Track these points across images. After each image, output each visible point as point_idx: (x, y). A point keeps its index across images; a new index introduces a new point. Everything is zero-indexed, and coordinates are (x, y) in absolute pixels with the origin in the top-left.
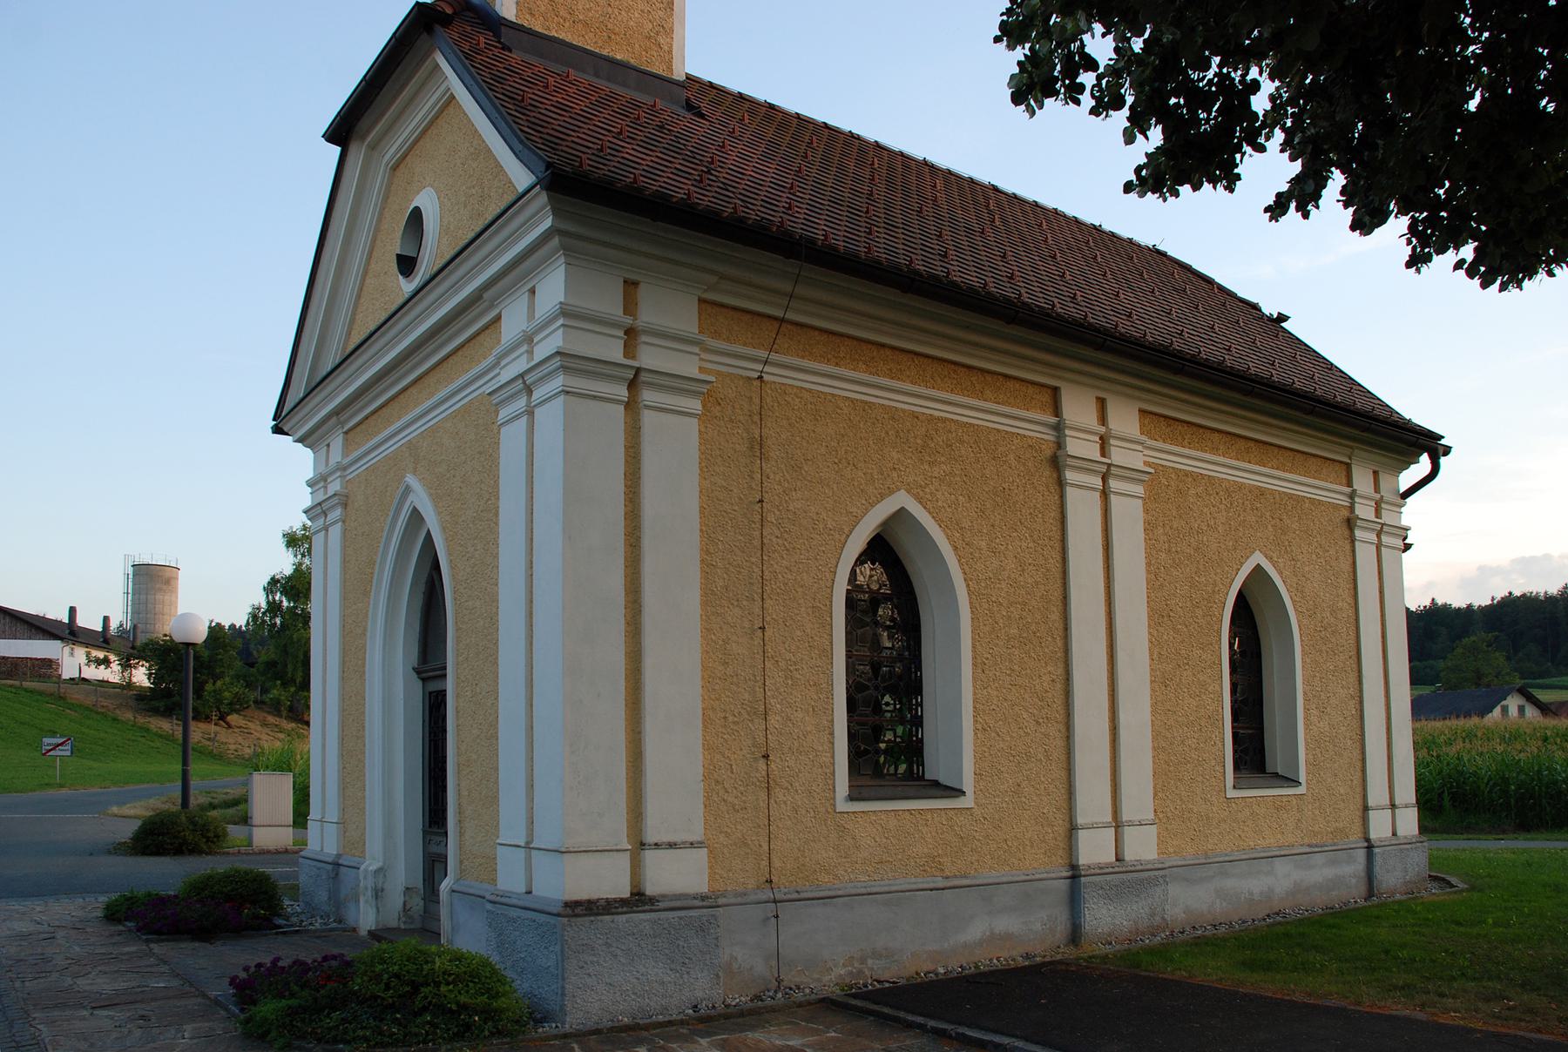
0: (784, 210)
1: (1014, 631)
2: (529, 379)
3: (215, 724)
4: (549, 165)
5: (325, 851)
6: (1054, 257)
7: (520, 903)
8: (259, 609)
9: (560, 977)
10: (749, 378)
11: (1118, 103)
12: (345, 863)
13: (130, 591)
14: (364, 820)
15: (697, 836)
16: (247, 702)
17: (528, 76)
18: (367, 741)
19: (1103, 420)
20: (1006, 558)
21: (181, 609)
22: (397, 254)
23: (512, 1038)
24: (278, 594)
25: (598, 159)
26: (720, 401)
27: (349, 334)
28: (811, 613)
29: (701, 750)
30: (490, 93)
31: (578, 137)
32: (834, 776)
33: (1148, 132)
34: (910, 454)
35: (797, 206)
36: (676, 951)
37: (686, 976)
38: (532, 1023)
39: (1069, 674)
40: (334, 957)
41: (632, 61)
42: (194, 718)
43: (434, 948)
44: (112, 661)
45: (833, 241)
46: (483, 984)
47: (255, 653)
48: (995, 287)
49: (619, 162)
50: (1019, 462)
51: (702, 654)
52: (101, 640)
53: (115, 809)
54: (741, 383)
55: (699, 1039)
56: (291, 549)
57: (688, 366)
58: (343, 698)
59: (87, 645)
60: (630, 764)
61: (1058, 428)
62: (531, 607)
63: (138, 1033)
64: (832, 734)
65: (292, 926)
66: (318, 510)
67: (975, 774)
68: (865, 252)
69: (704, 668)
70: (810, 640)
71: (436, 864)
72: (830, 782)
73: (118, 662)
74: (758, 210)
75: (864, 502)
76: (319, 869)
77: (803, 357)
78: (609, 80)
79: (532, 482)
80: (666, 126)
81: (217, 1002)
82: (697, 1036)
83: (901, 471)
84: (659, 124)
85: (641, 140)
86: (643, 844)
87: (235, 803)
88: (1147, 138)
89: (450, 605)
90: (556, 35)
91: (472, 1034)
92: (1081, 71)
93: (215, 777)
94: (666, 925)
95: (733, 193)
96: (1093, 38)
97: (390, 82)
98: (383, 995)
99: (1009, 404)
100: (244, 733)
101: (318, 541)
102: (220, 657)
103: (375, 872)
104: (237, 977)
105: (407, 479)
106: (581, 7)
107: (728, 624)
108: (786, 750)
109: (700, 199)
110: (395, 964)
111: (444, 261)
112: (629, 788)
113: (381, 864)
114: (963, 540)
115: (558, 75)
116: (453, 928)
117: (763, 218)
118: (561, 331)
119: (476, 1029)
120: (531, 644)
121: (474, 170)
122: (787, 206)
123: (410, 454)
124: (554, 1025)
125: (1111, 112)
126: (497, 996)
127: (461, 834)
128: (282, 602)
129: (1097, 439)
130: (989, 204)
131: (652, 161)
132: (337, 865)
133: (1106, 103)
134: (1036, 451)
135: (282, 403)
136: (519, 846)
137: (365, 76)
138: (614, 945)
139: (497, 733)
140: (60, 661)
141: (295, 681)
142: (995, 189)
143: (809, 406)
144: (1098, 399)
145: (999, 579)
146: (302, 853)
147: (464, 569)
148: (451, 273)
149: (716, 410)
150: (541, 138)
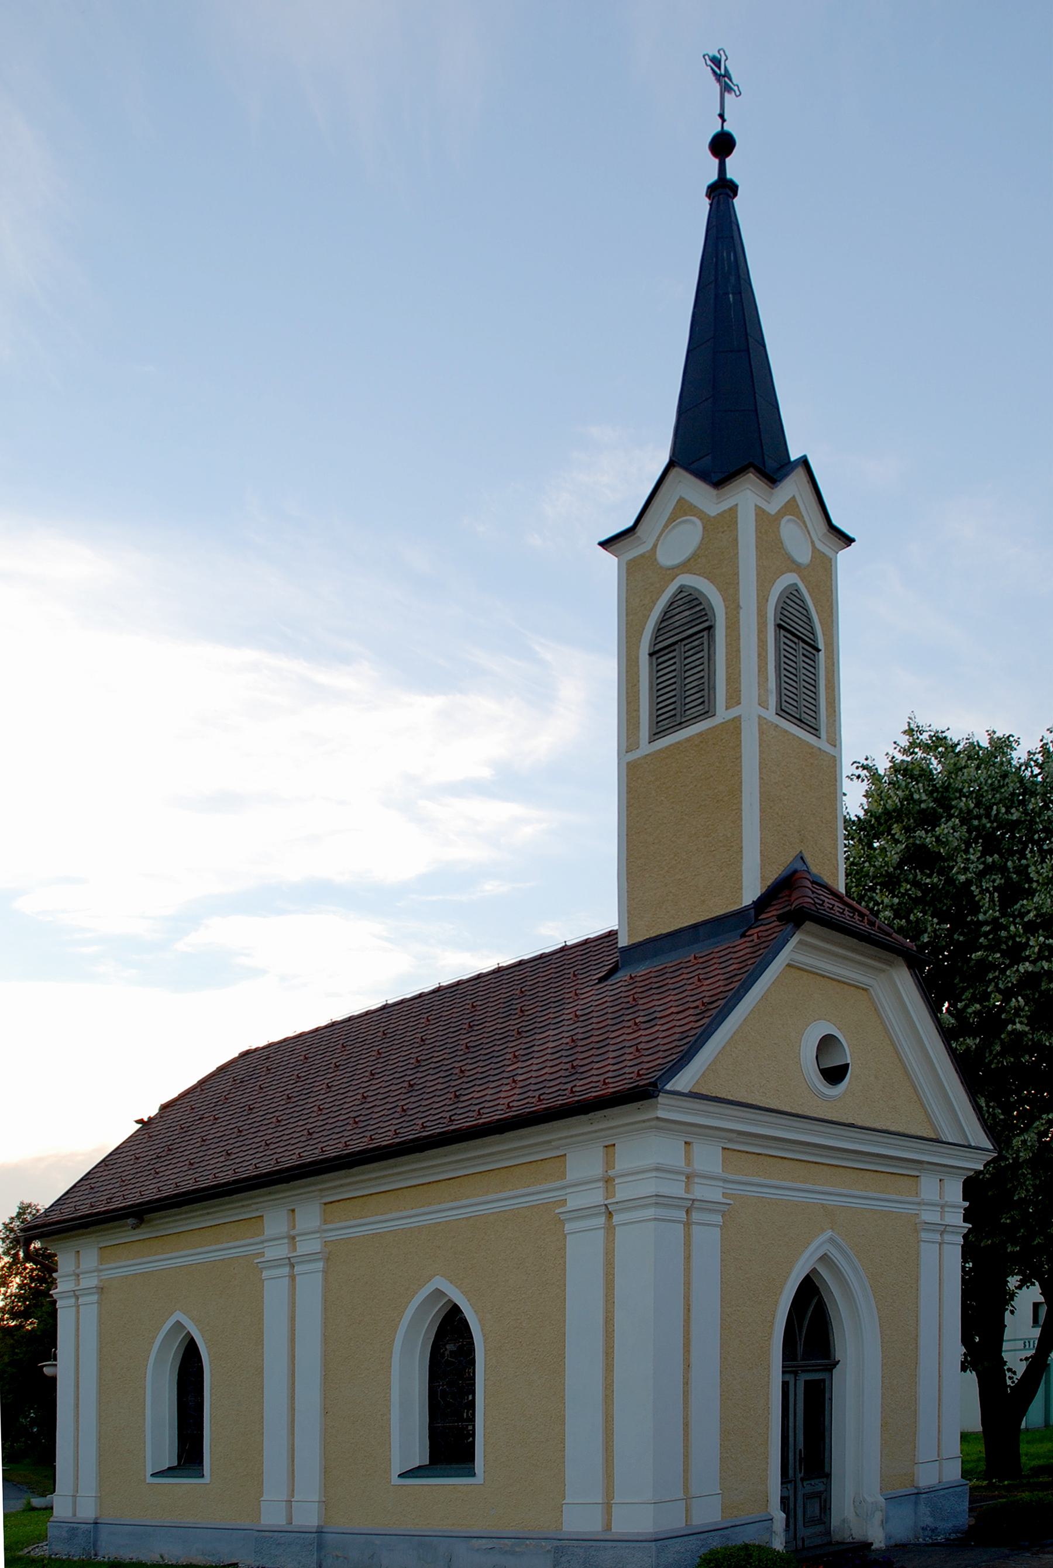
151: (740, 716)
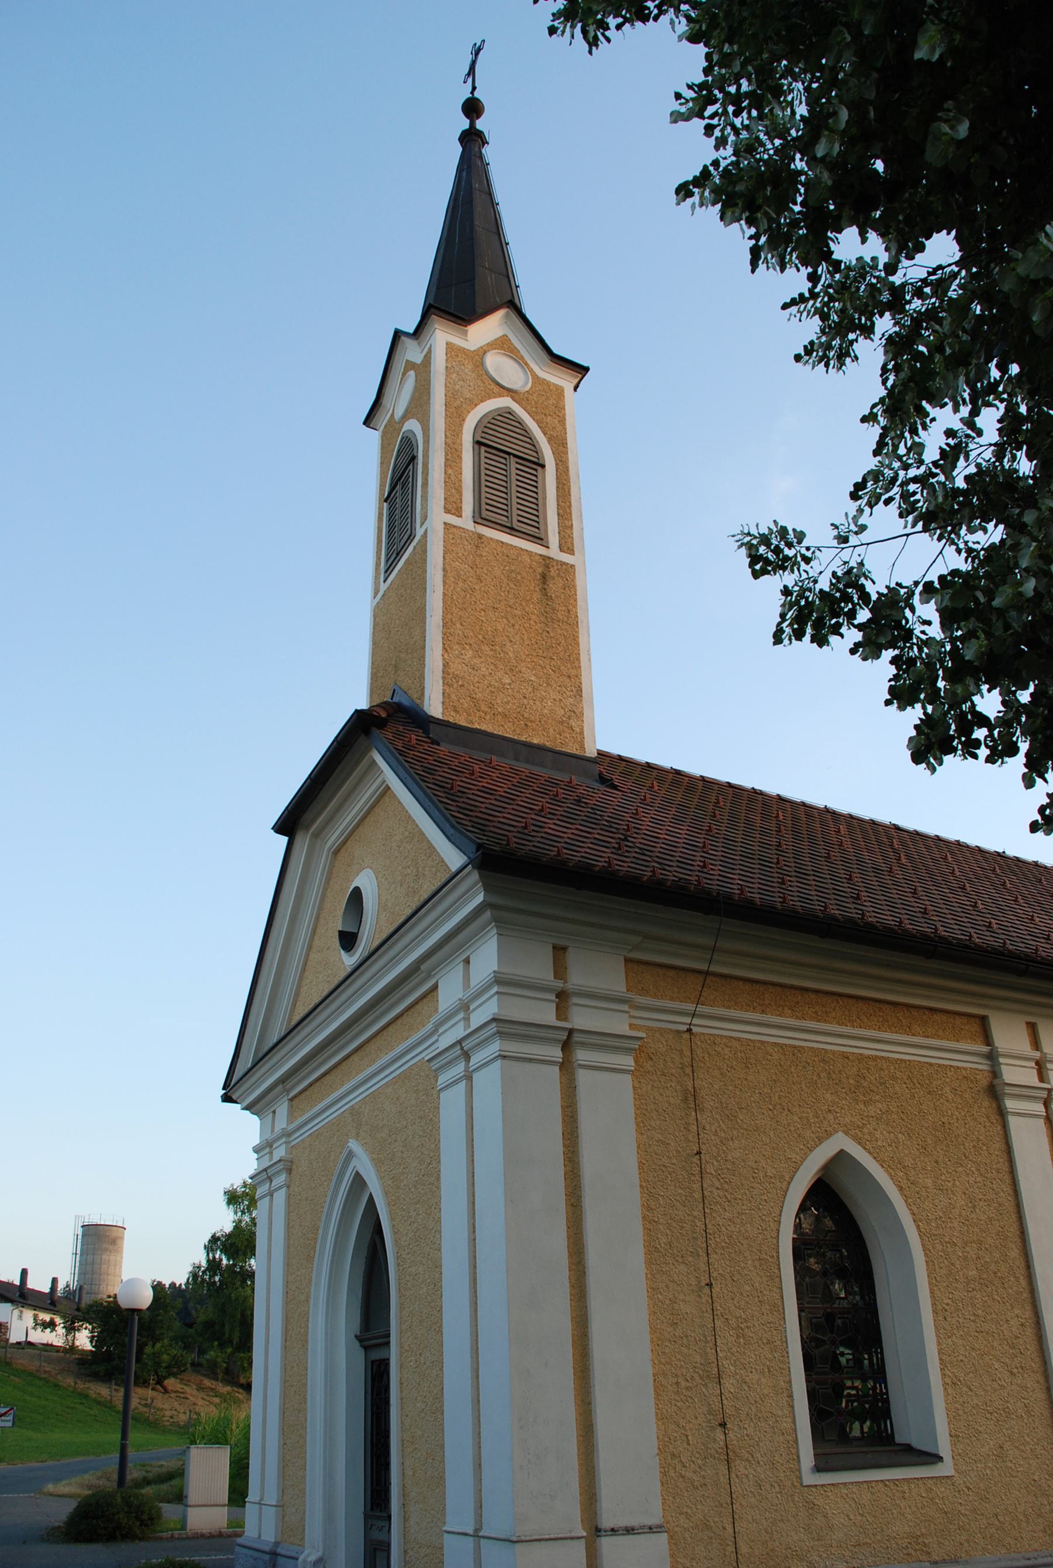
1: (973, 1273)
2: (467, 1045)
3: (153, 1389)
4: (479, 847)
5: (263, 1538)
6: (964, 888)
8: (199, 1267)
10: (678, 1032)
11: (1013, 751)
12: (283, 1552)
13: (79, 1252)
15: (655, 1519)
16: (185, 1364)
18: (308, 1417)
19: (1036, 1044)
20: (954, 1194)
21: (125, 1276)
22: (339, 931)
24: (218, 1252)
26: (652, 1055)
27: (294, 1005)
28: (758, 1265)
30: (423, 784)
31: (504, 817)
32: (797, 1444)
33: (1046, 775)
34: (844, 1095)
39: (1038, 1317)
41: (548, 744)
47: (193, 1312)
48: (911, 924)
50: (955, 1094)
51: (650, 1315)
52: (49, 1301)
53: (50, 1487)
54: (671, 1037)
56: (231, 1206)
57: (619, 1024)
59: (35, 1308)
61: (992, 1057)
62: (475, 1273)
64: (791, 1396)
66: (264, 1175)
67: (951, 1436)
68: (780, 902)
69: (653, 1330)
70: (760, 1294)
72: (793, 1451)
73: (62, 1325)
74: (676, 871)
75: (802, 1147)
76: (255, 1559)
77: (729, 1007)
78: (527, 762)
79: (473, 1145)
80: (584, 800)
83: (836, 1113)
86: (598, 1530)
88: (1046, 781)
89: (393, 1272)
90: (478, 727)
92: (976, 728)
93: (150, 1447)
96: (982, 697)
97: (332, 779)
99: (939, 1037)
100: (179, 1397)
102: (160, 1318)
103: (314, 1562)
105: (349, 1144)
106: (499, 701)
107: (674, 1281)
108: (743, 1417)
109: (620, 866)
111: (384, 936)
112: (580, 1465)
113: (320, 1554)
114: (908, 1180)
115: (482, 762)
117: (681, 879)
122: (702, 864)
123: (353, 1120)
125: (1006, 759)
127: (405, 1519)
128: (221, 1260)
129: (1033, 1064)
130: (892, 842)
131: (572, 833)
132: (274, 1554)
133: (1001, 751)
134: (972, 1081)
136: (466, 1534)
137: (310, 775)
139: (442, 1406)
140: (9, 1325)
142: (897, 828)
143: (739, 1054)
144: (1028, 1023)
145: (949, 1218)
146: (239, 1540)
147: (407, 1234)
149: (648, 1065)
150: (470, 821)
151: (574, 554)
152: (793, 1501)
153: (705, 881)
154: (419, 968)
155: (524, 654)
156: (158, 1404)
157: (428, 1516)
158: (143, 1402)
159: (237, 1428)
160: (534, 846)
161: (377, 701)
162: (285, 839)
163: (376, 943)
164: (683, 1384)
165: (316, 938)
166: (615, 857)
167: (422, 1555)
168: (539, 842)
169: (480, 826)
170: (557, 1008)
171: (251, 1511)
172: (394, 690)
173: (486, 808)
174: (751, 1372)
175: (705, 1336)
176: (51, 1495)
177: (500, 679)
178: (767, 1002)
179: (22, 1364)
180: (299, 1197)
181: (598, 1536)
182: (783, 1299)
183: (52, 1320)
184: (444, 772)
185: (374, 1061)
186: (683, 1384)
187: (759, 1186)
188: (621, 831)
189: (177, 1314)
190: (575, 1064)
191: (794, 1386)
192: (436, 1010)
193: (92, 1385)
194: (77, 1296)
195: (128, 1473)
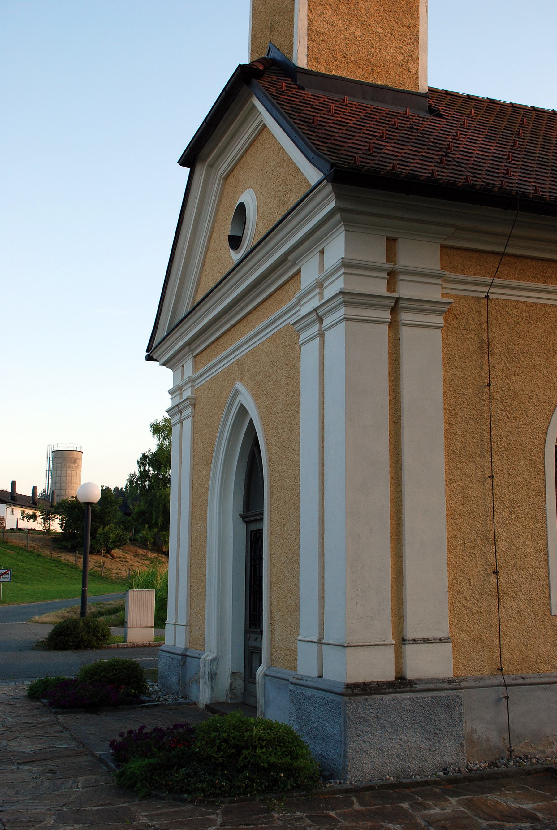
0: (503, 175)
4: (333, 165)
7: (314, 685)
8: (134, 476)
9: (343, 743)
10: (478, 298)
13: (51, 469)
14: (204, 623)
16: (125, 540)
17: (316, 105)
18: (207, 567)
22: (229, 236)
23: (307, 791)
24: (147, 466)
25: (366, 156)
27: (197, 290)
29: (447, 569)
30: (291, 120)
32: (549, 586)
35: (512, 171)
36: (430, 724)
37: (437, 744)
38: (322, 779)
40: (182, 726)
42: (91, 553)
43: (252, 719)
44: (38, 516)
45: (541, 193)
46: (287, 748)
49: (381, 157)
53: (37, 618)
54: (473, 302)
55: (449, 798)
58: (192, 506)
59: (22, 506)
60: (394, 580)
62: (323, 470)
63: (47, 783)
65: (153, 701)
66: (176, 409)
69: (449, 508)
71: (254, 655)
72: (546, 591)
73: (41, 517)
74: (484, 178)
76: (172, 659)
77: (519, 279)
78: (373, 100)
79: (323, 382)
80: (415, 127)
81: (100, 760)
82: (448, 795)
84: (409, 126)
85: (397, 139)
86: (404, 640)
87: (116, 611)
89: (266, 469)
90: (335, 74)
91: (278, 787)
94: (422, 703)
95: (465, 168)
97: (222, 121)
98: (215, 756)
100: (122, 561)
101: (175, 430)
104: (115, 740)
105: (236, 385)
106: (352, 52)
107: (465, 474)
110: (225, 732)
111: (261, 237)
112: (393, 597)
113: (215, 655)
115: (337, 101)
116: (265, 703)
117: (487, 183)
118: (343, 277)
119: (282, 783)
120: (323, 495)
121: (280, 173)
122: (505, 172)
123: (239, 369)
124: (338, 781)
126: (296, 757)
127: (272, 633)
128: (149, 471)
135: (152, 342)
138: (383, 718)
140: (5, 518)
141: (158, 524)
146: (161, 648)
147: (276, 445)
148: (266, 244)
149: (454, 323)
150: (326, 147)
152: (544, 625)
153: (506, 184)
154: (287, 259)
155: (374, 10)
156: (108, 565)
157: (287, 630)
158: (97, 565)
159: (161, 579)
160: (375, 164)
161: (256, 58)
162: (188, 170)
163: (255, 243)
164: (469, 544)
165: (212, 242)
166: (438, 169)
167: (283, 655)
168: (378, 160)
169: (333, 150)
170: (388, 281)
171: (169, 628)
172: (270, 48)
173: (339, 136)
174: (519, 537)
175: (486, 512)
176: (37, 622)
177: (353, 33)
178: (549, 274)
179: (14, 543)
180: (201, 423)
181: (403, 644)
182: (545, 487)
183: (34, 514)
184: (307, 110)
185: (254, 327)
186: (469, 544)
187: (533, 408)
188: (443, 150)
189: (119, 507)
190: (400, 323)
191: (549, 547)
192: (299, 288)
193: (62, 555)
194: (51, 498)
195: (87, 608)
